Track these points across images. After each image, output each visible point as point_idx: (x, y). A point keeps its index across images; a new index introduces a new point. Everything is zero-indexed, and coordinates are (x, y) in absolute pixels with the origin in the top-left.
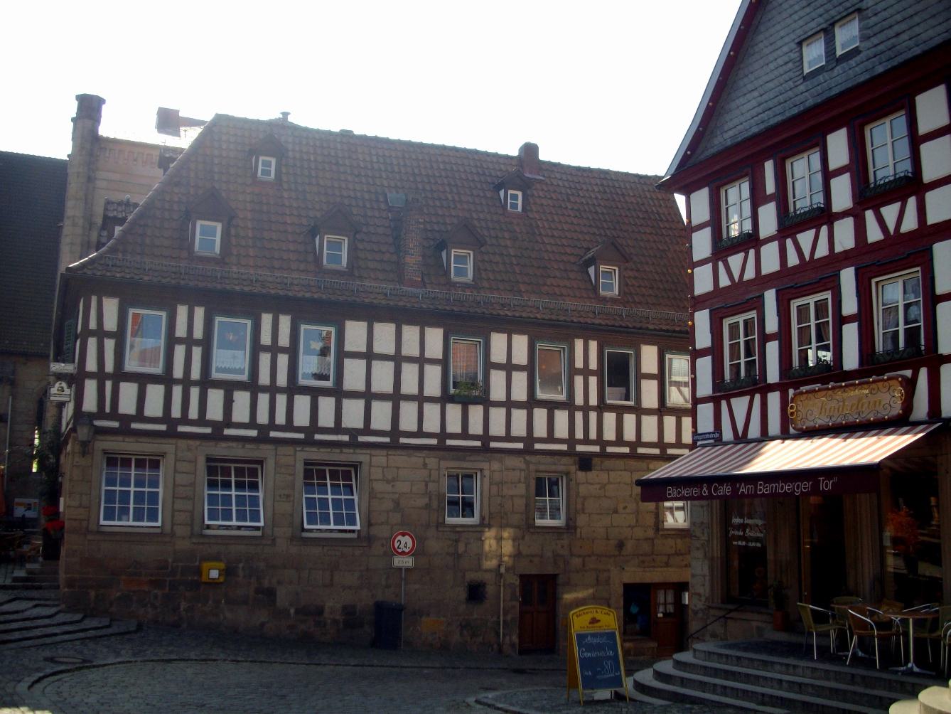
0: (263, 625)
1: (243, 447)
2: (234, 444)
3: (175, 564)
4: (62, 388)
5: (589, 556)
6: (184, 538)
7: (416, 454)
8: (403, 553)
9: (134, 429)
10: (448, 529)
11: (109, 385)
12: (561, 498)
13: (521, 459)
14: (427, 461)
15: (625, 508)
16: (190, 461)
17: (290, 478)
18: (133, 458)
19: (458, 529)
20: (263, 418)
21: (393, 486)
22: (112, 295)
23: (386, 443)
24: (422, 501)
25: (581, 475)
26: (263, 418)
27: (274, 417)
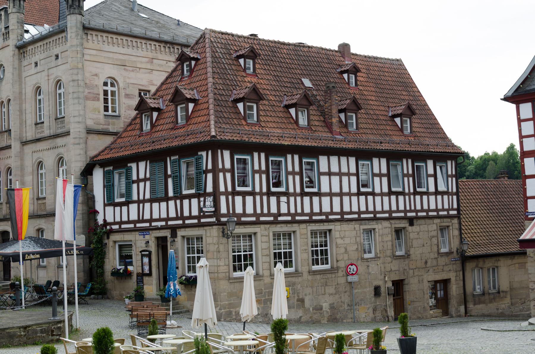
0: (301, 317)
1: (287, 226)
2: (283, 225)
5: (415, 269)
7: (351, 223)
8: (352, 274)
9: (330, 219)
10: (365, 260)
11: (230, 197)
12: (401, 241)
13: (389, 222)
14: (356, 226)
15: (427, 243)
16: (266, 236)
17: (306, 240)
18: (282, 233)
20: (274, 210)
21: (344, 240)
22: (226, 149)
23: (339, 219)
24: (355, 247)
25: (410, 228)
26: (274, 210)
27: (280, 210)
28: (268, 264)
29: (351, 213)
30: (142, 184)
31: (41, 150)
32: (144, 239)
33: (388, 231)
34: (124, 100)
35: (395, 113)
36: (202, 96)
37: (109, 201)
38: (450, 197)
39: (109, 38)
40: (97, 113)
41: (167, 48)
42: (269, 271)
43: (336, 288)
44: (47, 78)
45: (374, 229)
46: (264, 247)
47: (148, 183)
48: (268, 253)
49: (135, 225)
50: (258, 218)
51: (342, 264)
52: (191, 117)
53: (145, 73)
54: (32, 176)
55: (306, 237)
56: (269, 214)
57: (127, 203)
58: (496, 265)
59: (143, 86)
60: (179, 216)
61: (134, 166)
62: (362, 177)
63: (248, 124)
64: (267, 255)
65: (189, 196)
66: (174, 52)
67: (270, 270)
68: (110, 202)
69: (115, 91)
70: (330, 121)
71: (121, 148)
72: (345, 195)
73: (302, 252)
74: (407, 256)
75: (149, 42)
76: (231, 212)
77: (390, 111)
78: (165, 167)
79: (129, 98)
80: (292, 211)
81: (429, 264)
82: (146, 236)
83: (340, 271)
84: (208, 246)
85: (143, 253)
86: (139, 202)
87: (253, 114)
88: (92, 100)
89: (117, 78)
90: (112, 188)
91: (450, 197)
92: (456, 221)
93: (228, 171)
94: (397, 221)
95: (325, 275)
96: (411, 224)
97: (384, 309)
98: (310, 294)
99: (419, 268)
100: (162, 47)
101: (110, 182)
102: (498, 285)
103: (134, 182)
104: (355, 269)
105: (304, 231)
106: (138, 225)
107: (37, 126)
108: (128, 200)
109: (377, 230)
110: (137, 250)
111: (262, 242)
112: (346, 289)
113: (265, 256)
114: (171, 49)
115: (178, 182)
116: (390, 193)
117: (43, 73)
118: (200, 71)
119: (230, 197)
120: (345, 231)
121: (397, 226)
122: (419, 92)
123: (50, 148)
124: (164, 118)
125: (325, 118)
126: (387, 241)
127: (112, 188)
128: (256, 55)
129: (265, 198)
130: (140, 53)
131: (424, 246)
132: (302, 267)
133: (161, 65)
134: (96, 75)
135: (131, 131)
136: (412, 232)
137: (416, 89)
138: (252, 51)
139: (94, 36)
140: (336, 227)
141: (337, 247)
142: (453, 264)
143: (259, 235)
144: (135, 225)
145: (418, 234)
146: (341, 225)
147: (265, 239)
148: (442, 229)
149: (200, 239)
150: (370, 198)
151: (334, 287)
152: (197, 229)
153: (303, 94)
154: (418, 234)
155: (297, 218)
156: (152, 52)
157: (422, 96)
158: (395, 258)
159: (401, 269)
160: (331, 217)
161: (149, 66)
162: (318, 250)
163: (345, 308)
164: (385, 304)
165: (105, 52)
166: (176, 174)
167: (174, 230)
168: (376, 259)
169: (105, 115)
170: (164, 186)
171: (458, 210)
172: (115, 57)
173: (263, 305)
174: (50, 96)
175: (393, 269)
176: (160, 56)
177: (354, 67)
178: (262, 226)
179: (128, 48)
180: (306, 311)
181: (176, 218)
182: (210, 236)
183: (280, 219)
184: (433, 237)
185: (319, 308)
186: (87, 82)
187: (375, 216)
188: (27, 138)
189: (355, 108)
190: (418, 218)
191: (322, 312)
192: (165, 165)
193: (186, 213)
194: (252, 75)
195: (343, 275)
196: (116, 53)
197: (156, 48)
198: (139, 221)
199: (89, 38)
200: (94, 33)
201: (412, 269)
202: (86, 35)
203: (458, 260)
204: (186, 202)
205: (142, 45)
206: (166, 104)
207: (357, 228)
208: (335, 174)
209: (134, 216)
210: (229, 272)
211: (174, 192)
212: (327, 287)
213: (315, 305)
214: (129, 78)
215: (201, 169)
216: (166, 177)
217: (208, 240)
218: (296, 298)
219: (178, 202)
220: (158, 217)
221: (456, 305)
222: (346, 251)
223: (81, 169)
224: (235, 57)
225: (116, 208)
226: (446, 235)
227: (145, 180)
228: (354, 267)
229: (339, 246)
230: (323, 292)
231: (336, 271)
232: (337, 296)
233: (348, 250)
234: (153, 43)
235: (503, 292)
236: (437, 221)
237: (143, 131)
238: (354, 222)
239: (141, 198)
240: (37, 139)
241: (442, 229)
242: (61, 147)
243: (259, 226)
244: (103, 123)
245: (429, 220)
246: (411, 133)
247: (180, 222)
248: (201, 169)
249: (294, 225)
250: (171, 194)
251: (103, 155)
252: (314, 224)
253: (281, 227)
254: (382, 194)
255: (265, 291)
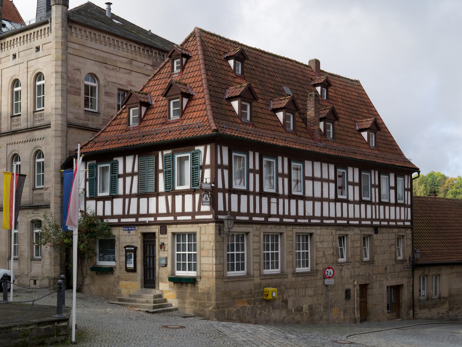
1: (275, 228)
2: (272, 226)
3: (255, 291)
4: (207, 197)
6: (257, 277)
8: (329, 277)
9: (312, 223)
10: (339, 264)
11: (227, 195)
12: (367, 247)
13: (359, 229)
15: (387, 251)
17: (291, 242)
18: (270, 234)
19: (342, 264)
20: (265, 211)
21: (323, 244)
24: (331, 251)
25: (375, 236)
26: (265, 211)
28: (258, 264)
29: (148, 215)
30: (128, 179)
31: (16, 142)
32: (129, 234)
33: (357, 237)
34: (104, 98)
35: (362, 127)
36: (197, 92)
37: (92, 195)
38: (406, 209)
39: (92, 34)
40: (78, 108)
41: (146, 50)
42: (259, 272)
43: (314, 290)
44: (26, 70)
45: (347, 235)
46: (255, 247)
47: (136, 178)
48: (258, 253)
49: (119, 220)
50: (251, 218)
51: (320, 267)
52: (185, 112)
53: (125, 73)
54: (6, 168)
55: (292, 240)
56: (261, 215)
57: (111, 198)
58: (439, 273)
59: (122, 85)
60: (170, 212)
61: (120, 161)
62: (339, 184)
63: (243, 123)
64: (258, 256)
65: (183, 192)
66: (152, 55)
67: (260, 270)
68: (92, 196)
69: (95, 87)
70: (312, 128)
71: (107, 141)
72: (325, 201)
73: (288, 254)
74: (371, 262)
75: (129, 43)
76: (227, 210)
77: (357, 125)
78: (156, 161)
79: (108, 96)
80: (281, 213)
81: (388, 270)
82: (131, 231)
83: (318, 274)
84: (202, 243)
85: (127, 248)
86: (124, 196)
87: (247, 113)
88: (73, 94)
89: (98, 75)
90: (95, 182)
91: (406, 209)
92: (409, 231)
93: (225, 167)
94: (366, 229)
95: (306, 277)
96: (376, 232)
97: (352, 311)
98: (293, 295)
99: (380, 274)
100: (141, 49)
101: (93, 176)
102: (439, 291)
103: (119, 176)
104: (332, 273)
105: (290, 233)
106: (123, 220)
107: (13, 119)
108: (112, 194)
109: (350, 236)
110: (121, 245)
111: (254, 242)
112: (323, 292)
113: (256, 256)
114: (150, 52)
115: (170, 177)
116: (361, 202)
117: (22, 65)
118: (192, 68)
119: (227, 195)
120: (324, 235)
121: (365, 233)
122: (376, 111)
123: (26, 141)
124: (109, 131)
125: (306, 125)
126: (357, 247)
127: (95, 182)
128: (245, 58)
129: (257, 198)
130: (121, 53)
131: (385, 253)
132: (288, 269)
133: (139, 67)
134: (78, 70)
135: (116, 125)
136: (377, 240)
137: (373, 109)
138: (242, 53)
139: (78, 30)
140: (317, 231)
141: (317, 251)
142: (406, 271)
143: (251, 235)
144: (119, 220)
145: (381, 242)
146: (321, 229)
147: (256, 239)
148: (399, 238)
149: (192, 235)
150: (345, 205)
151: (313, 289)
152: (190, 225)
153: (291, 99)
154: (381, 242)
155: (285, 220)
156: (132, 53)
157: (379, 115)
158: (362, 263)
159: (367, 274)
160: (313, 221)
161: (128, 67)
162: (234, 254)
163: (321, 310)
164: (353, 307)
165: (88, 48)
166: (169, 169)
167: (163, 226)
168: (348, 264)
169: (85, 110)
170: (154, 181)
171: (411, 221)
172: (97, 54)
173: (252, 306)
174: (29, 89)
175: (360, 274)
176: (139, 59)
177: (327, 81)
178: (255, 226)
179: (110, 47)
180: (289, 312)
181: (167, 214)
182: (205, 234)
183: (270, 220)
184: (392, 245)
185: (299, 310)
186: (70, 75)
187: (348, 222)
188: (2, 131)
189: (333, 118)
190: (381, 226)
191: (302, 313)
192: (156, 159)
193: (178, 209)
194: (241, 77)
195: (321, 277)
196: (98, 50)
197: (135, 50)
198: (124, 216)
199: (73, 31)
200: (78, 27)
201: (375, 274)
202: (70, 28)
203: (410, 267)
204: (179, 198)
205: (123, 45)
206: (155, 100)
207: (334, 234)
208: (318, 180)
209: (118, 211)
210: (223, 271)
211: (166, 187)
212: (307, 289)
213: (297, 306)
214: (109, 76)
215: (197, 164)
216: (157, 172)
217: (202, 237)
218: (281, 299)
219: (170, 198)
220: (145, 212)
221: (407, 309)
222: (324, 255)
223: (61, 162)
224: (224, 58)
225: (98, 202)
226: (367, 244)
227: (132, 174)
228: (331, 270)
229: (319, 250)
230: (304, 294)
231: (315, 274)
232: (315, 298)
233: (326, 254)
234: (133, 44)
235: (443, 298)
236: (396, 230)
237: (130, 126)
238: (330, 228)
239: (127, 192)
240: (12, 132)
241: (399, 238)
242: (39, 140)
243: (251, 226)
244: (83, 118)
245: (389, 229)
246: (375, 147)
247: (171, 218)
248: (197, 164)
249: (282, 227)
250: (162, 188)
251: (86, 148)
252: (298, 227)
253: (271, 228)
254: (354, 202)
255: (255, 291)
